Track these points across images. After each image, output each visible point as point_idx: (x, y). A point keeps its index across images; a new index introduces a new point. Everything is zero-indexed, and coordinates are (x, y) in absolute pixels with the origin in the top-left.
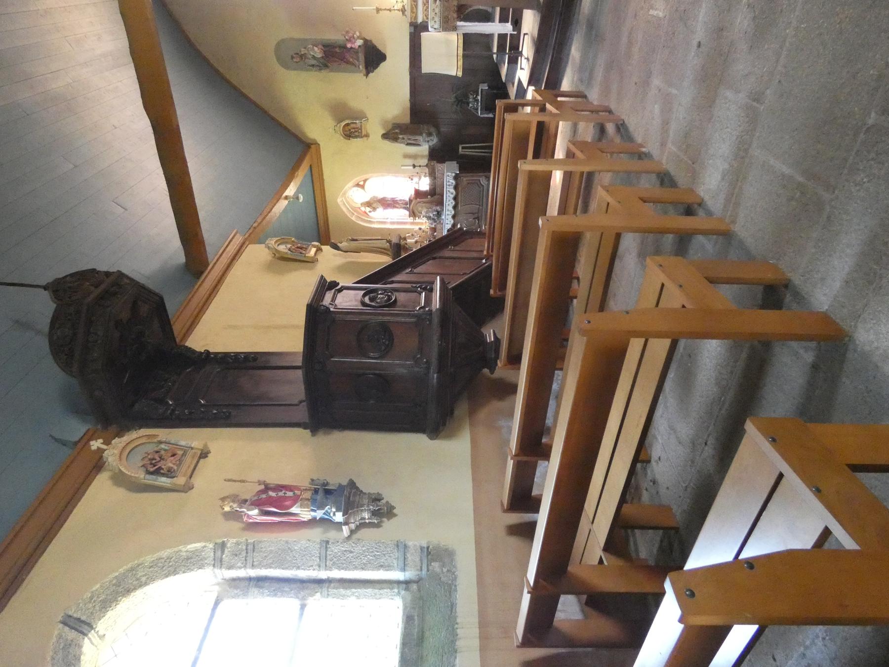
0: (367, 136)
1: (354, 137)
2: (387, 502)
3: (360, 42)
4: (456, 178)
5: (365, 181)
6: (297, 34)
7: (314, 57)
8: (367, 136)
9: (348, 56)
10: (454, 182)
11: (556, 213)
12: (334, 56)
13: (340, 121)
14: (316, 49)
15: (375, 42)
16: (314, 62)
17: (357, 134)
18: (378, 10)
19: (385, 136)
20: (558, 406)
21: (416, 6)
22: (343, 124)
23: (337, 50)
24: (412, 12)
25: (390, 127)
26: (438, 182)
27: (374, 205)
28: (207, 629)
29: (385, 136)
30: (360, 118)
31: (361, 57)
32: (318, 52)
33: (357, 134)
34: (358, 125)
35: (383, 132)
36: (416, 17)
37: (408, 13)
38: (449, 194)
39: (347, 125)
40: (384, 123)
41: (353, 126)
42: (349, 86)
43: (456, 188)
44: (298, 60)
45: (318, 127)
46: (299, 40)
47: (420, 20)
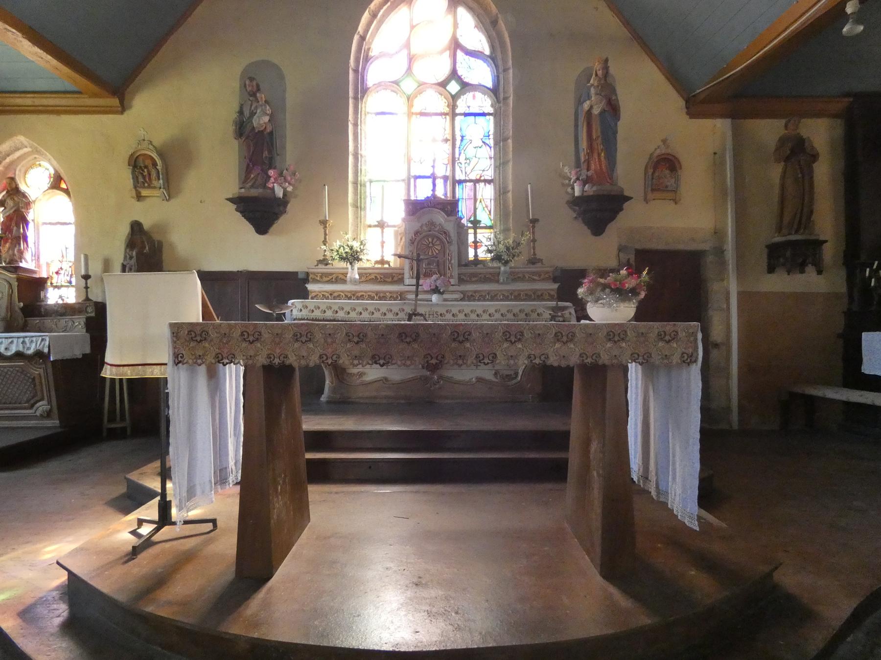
0: (139, 197)
1: (133, 172)
2: (477, 378)
3: (279, 193)
4: (39, 354)
5: (67, 191)
6: (292, 98)
7: (253, 114)
8: (139, 197)
9: (257, 170)
10: (30, 352)
11: (306, 427)
12: (259, 148)
13: (161, 155)
14: (266, 119)
15: (282, 220)
16: (247, 113)
17: (141, 179)
18: (324, 223)
19: (136, 227)
20: (192, 449)
21: (330, 282)
22: (154, 155)
23: (266, 154)
24: (323, 275)
25: (156, 237)
26: (48, 322)
27: (10, 203)
28: (50, 224)
29: (136, 227)
30: (167, 185)
31: (254, 192)
32: (261, 120)
33: (141, 179)
34: (155, 183)
35: (146, 224)
36: (316, 281)
37: (322, 269)
38: (6, 342)
39: (155, 164)
40: (162, 228)
41: (154, 174)
42: (217, 173)
43: (19, 355)
44: (249, 89)
45: (152, 113)
46: (284, 100)
47: (310, 287)
